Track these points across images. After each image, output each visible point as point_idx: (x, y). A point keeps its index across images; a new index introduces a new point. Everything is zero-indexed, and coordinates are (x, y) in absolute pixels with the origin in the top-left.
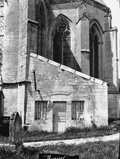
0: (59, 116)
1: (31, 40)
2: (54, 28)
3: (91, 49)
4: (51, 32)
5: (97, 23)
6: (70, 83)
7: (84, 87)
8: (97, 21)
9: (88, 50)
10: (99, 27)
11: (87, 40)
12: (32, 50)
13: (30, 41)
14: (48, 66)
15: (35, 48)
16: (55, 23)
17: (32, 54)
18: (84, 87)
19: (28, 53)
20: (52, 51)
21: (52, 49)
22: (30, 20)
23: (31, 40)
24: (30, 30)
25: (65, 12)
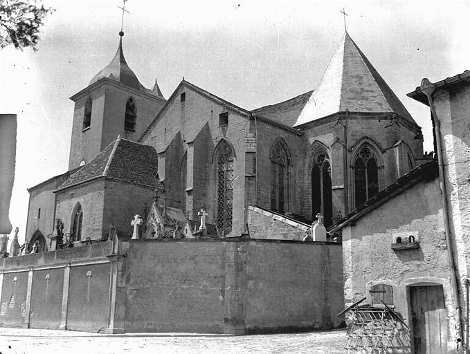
0: (116, 251)
1: (248, 193)
2: (310, 160)
3: (346, 184)
4: (306, 166)
5: (369, 142)
6: (281, 232)
7: (293, 235)
8: (367, 138)
9: (342, 187)
10: (375, 146)
11: (340, 173)
12: (250, 203)
13: (248, 194)
14: (262, 217)
15: (253, 200)
16: (310, 152)
17: (251, 208)
18: (293, 235)
19: (246, 207)
20: (311, 190)
21: (311, 187)
22: (247, 175)
23: (248, 193)
24: (247, 185)
25: (320, 138)
